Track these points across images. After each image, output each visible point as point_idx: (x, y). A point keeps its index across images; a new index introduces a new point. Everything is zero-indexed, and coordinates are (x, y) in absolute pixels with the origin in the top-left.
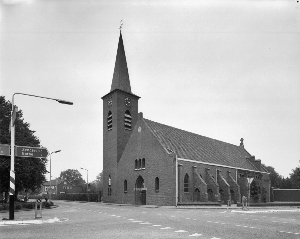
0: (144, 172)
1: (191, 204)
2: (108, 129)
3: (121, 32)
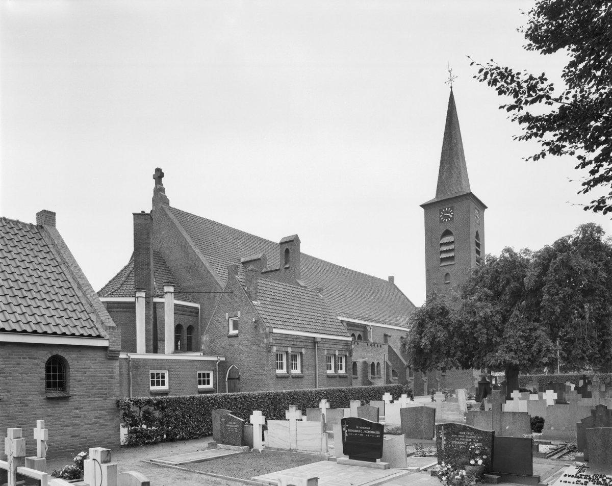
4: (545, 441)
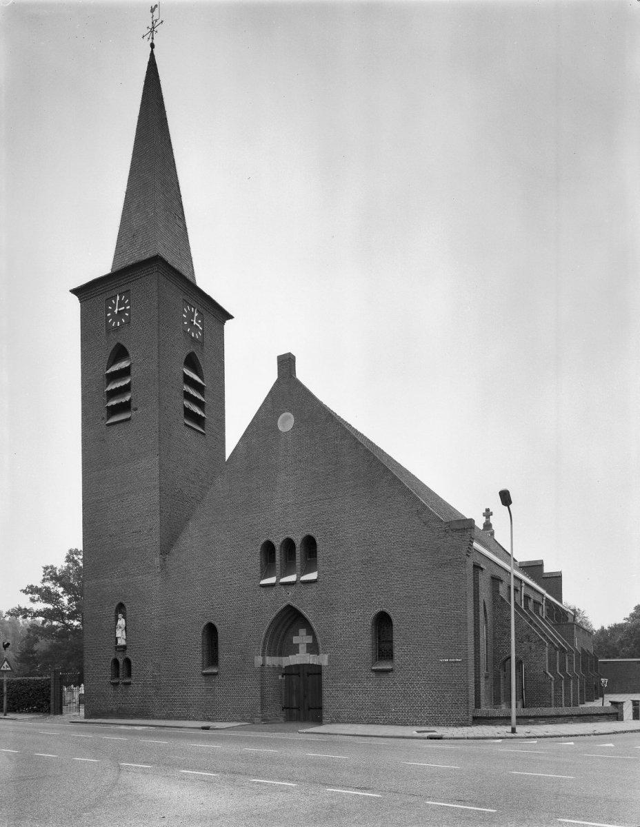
0: (312, 591)
1: (534, 717)
2: (108, 418)
3: (152, 51)
4: (136, 728)
